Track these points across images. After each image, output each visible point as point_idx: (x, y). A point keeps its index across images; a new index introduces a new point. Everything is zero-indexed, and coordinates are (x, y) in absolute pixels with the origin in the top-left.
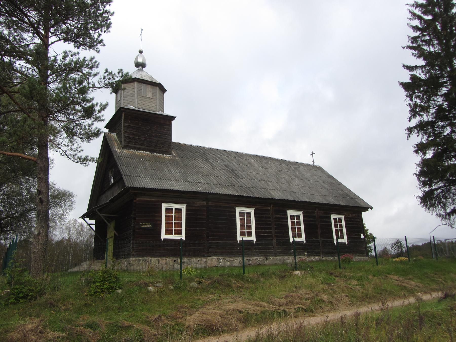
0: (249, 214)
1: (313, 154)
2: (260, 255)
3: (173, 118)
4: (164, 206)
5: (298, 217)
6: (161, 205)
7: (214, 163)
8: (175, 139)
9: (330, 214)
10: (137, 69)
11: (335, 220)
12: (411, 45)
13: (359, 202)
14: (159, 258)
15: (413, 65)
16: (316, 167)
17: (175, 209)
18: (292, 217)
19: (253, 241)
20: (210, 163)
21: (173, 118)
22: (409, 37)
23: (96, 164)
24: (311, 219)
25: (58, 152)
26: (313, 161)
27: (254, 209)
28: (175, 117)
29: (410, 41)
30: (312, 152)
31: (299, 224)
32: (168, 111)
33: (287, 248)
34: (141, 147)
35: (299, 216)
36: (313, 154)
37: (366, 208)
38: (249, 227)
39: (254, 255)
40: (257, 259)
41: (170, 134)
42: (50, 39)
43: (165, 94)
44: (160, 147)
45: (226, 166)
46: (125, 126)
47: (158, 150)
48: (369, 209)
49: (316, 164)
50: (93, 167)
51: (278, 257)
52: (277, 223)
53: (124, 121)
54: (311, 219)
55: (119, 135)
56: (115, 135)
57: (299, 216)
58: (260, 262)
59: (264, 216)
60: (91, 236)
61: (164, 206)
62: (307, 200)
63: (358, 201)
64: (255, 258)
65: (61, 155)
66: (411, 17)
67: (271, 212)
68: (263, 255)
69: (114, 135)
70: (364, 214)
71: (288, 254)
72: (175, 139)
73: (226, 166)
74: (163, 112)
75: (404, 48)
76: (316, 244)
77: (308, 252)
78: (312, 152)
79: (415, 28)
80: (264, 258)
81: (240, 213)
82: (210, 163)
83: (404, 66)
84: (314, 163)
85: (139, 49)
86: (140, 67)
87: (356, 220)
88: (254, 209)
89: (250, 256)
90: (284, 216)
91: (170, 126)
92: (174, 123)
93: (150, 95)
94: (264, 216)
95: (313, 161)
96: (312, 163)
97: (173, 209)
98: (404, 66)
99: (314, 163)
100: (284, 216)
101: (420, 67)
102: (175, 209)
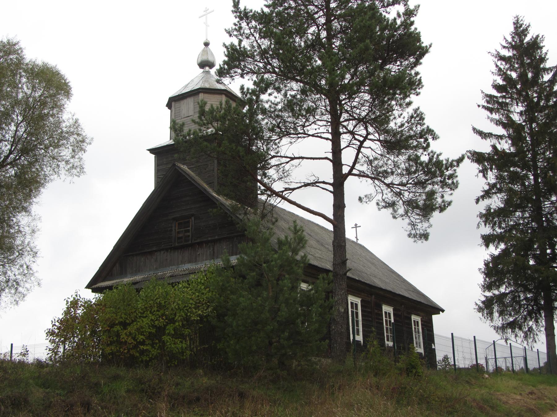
9: (411, 314)
10: (202, 70)
12: (486, 104)
15: (486, 131)
22: (482, 92)
26: (356, 238)
27: (360, 299)
29: (485, 100)
30: (356, 225)
37: (438, 310)
49: (359, 242)
66: (495, 71)
70: (434, 317)
75: (207, 44)
78: (356, 225)
79: (497, 87)
83: (474, 129)
85: (204, 40)
86: (207, 68)
88: (360, 299)
96: (355, 240)
98: (474, 129)
99: (357, 239)
101: (495, 135)
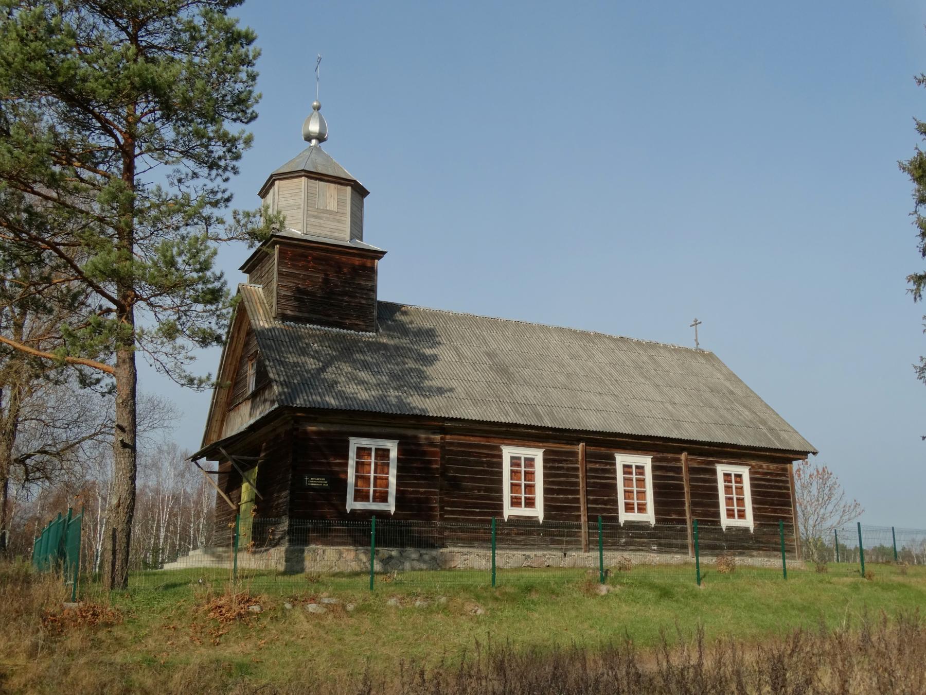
0: (530, 462)
1: (697, 323)
2: (552, 546)
3: (379, 255)
4: (355, 443)
5: (640, 469)
6: (348, 442)
7: (466, 351)
8: (384, 294)
11: (727, 476)
13: (787, 437)
14: (340, 548)
16: (702, 353)
17: (376, 449)
18: (627, 468)
19: (648, 522)
20: (456, 349)
21: (379, 255)
23: (212, 390)
24: (671, 474)
25: (153, 367)
26: (696, 340)
28: (384, 253)
31: (515, 487)
32: (369, 243)
33: (608, 531)
34: (314, 316)
35: (642, 468)
36: (697, 323)
38: (530, 488)
39: (539, 548)
40: (544, 555)
41: (373, 289)
42: (136, 160)
43: (366, 200)
44: (352, 315)
45: (490, 355)
46: (280, 274)
47: (348, 322)
48: (810, 455)
50: (208, 394)
51: (591, 554)
52: (707, 476)
53: (279, 263)
54: (671, 474)
55: (266, 287)
56: (260, 289)
57: (642, 468)
58: (550, 562)
59: (565, 465)
60: (420, 559)
61: (355, 443)
62: (661, 433)
63: (784, 435)
64: (539, 553)
65: (158, 370)
67: (581, 457)
68: (557, 546)
69: (259, 289)
71: (615, 546)
72: (384, 294)
73: (490, 355)
74: (361, 240)
76: (679, 527)
77: (659, 545)
80: (561, 554)
81: (512, 458)
82: (456, 349)
84: (698, 344)
87: (779, 478)
89: (530, 549)
90: (608, 467)
91: (373, 271)
92: (380, 264)
93: (332, 205)
94: (565, 465)
95: (696, 340)
97: (371, 449)
99: (698, 344)
100: (608, 467)
102: (376, 449)
